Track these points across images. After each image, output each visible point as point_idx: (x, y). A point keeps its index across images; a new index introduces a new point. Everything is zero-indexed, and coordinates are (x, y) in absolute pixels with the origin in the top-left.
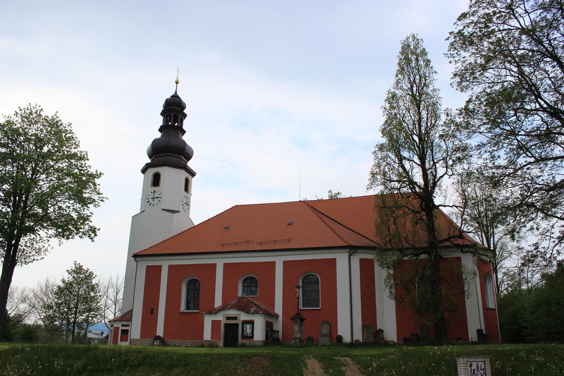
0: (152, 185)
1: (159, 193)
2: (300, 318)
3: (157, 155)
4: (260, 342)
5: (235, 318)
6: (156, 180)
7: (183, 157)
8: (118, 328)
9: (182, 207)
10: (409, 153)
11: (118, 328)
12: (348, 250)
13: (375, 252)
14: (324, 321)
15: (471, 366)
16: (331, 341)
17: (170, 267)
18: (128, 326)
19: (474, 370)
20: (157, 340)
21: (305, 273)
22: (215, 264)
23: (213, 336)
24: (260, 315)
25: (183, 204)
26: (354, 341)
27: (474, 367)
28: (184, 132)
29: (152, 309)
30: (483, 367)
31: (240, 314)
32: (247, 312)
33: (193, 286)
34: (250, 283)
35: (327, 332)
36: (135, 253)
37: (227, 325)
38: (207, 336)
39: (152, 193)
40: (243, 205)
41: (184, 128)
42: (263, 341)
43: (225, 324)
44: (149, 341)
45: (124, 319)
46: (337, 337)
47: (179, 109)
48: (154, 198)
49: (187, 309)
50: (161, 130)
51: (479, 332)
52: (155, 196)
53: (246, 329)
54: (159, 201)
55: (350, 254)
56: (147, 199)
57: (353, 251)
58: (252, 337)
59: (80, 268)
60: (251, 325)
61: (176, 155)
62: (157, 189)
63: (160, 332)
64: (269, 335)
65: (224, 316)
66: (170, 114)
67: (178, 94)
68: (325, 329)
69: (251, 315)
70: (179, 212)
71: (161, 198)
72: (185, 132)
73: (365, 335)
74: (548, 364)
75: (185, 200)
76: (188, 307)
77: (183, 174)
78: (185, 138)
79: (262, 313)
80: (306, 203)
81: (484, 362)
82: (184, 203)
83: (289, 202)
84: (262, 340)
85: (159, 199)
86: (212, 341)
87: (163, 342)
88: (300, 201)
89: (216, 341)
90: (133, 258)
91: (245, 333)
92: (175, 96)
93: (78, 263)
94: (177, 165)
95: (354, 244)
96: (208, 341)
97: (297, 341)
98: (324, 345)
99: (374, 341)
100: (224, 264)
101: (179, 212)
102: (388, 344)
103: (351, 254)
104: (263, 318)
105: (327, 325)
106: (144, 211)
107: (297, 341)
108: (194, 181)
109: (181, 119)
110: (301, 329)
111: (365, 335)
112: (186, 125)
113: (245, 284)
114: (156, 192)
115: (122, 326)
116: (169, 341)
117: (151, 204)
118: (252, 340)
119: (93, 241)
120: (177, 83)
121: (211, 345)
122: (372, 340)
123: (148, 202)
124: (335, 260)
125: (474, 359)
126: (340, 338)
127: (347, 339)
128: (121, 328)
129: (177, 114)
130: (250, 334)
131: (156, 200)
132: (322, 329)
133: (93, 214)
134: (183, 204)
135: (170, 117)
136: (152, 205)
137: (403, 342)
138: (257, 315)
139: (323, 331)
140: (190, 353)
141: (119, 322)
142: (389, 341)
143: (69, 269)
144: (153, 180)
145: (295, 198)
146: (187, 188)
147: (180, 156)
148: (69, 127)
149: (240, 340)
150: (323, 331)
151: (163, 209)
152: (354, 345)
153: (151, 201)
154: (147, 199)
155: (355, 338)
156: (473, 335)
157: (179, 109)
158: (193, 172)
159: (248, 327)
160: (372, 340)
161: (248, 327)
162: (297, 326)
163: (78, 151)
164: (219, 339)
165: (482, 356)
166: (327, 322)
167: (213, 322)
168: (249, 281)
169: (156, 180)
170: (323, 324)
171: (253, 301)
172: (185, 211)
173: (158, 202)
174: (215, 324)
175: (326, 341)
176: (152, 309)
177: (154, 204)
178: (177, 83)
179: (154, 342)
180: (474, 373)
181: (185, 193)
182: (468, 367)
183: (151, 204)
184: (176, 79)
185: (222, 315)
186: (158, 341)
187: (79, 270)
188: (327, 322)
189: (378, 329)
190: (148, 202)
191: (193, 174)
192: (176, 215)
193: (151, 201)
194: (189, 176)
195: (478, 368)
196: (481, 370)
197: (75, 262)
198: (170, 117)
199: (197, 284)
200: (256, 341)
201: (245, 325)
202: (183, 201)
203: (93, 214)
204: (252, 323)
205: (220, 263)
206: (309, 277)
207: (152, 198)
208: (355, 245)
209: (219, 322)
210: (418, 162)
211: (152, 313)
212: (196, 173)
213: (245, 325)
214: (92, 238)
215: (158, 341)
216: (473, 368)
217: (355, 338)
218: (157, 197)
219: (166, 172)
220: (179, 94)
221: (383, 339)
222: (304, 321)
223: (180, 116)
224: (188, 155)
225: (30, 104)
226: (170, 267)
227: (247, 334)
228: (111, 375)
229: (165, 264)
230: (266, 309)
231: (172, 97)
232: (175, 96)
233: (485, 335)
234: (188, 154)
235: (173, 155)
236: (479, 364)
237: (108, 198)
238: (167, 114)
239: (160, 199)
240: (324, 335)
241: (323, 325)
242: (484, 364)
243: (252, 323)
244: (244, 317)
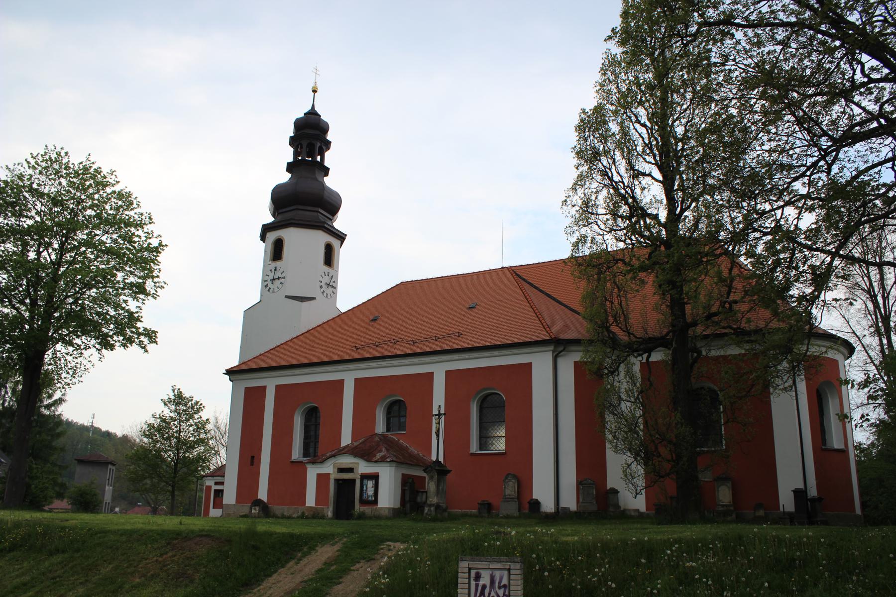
1: (281, 271)
3: (281, 211)
4: (387, 511)
5: (351, 470)
6: (277, 252)
8: (210, 487)
9: (319, 291)
11: (210, 487)
12: (552, 348)
13: (581, 348)
15: (478, 577)
16: (519, 510)
18: (222, 483)
19: (484, 587)
21: (481, 391)
23: (317, 503)
24: (388, 464)
25: (321, 287)
26: (560, 510)
27: (485, 580)
28: (326, 171)
29: (253, 457)
30: (505, 581)
33: (312, 415)
34: (396, 411)
35: (515, 494)
37: (341, 482)
38: (311, 500)
39: (272, 272)
40: (412, 281)
41: (327, 163)
42: (394, 509)
43: (337, 480)
45: (218, 473)
46: (529, 503)
47: (317, 132)
48: (274, 279)
49: (481, 450)
50: (290, 167)
51: (800, 494)
53: (367, 488)
54: (282, 283)
55: (556, 353)
56: (265, 281)
57: (561, 348)
58: (375, 502)
61: (309, 208)
62: (278, 264)
64: (407, 498)
65: (334, 467)
67: (316, 109)
68: (511, 489)
70: (313, 299)
71: (283, 278)
72: (329, 169)
73: (581, 500)
74: (697, 576)
75: (326, 279)
77: (320, 238)
78: (329, 181)
79: (391, 461)
81: (509, 570)
82: (323, 284)
83: (485, 271)
84: (392, 506)
85: (281, 280)
87: (265, 510)
88: (503, 268)
89: (323, 509)
91: (365, 496)
92: (312, 113)
93: (177, 387)
94: (297, 222)
95: (562, 334)
96: (311, 507)
97: (432, 509)
98: (507, 517)
100: (356, 380)
101: (313, 299)
103: (558, 354)
104: (393, 469)
105: (513, 481)
107: (432, 509)
109: (320, 148)
111: (581, 500)
112: (329, 159)
114: (278, 269)
115: (216, 483)
117: (270, 288)
118: (375, 507)
119: (146, 351)
120: (315, 91)
121: (316, 515)
122: (594, 507)
123: (266, 286)
124: (529, 366)
125: (484, 564)
126: (536, 504)
127: (548, 506)
129: (313, 142)
130: (372, 497)
131: (277, 282)
132: (505, 487)
133: (141, 309)
134: (321, 287)
135: (301, 148)
137: (654, 512)
139: (508, 492)
142: (629, 510)
143: (166, 398)
145: (496, 265)
147: (316, 209)
148: (113, 177)
150: (508, 492)
151: (287, 297)
152: (560, 516)
154: (265, 281)
155: (563, 504)
156: (787, 502)
157: (317, 132)
158: (339, 234)
160: (594, 507)
161: (370, 484)
162: (433, 483)
163: (135, 213)
164: (327, 505)
166: (515, 477)
168: (396, 408)
170: (507, 478)
171: (399, 440)
173: (280, 286)
174: (322, 479)
175: (511, 509)
176: (253, 457)
177: (274, 289)
178: (315, 91)
179: (251, 509)
180: (482, 592)
183: (270, 288)
184: (312, 85)
185: (332, 466)
186: (257, 508)
187: (179, 399)
188: (515, 477)
189: (608, 488)
191: (341, 237)
192: (312, 302)
193: (269, 283)
194: (335, 242)
195: (492, 582)
196: (500, 588)
197: (173, 387)
198: (301, 148)
200: (382, 508)
201: (365, 481)
202: (321, 282)
203: (141, 309)
205: (349, 377)
206: (490, 397)
207: (271, 280)
208: (562, 337)
210: (659, 176)
211: (252, 464)
212: (346, 235)
213: (365, 481)
214: (144, 348)
215: (257, 508)
216: (481, 582)
217: (563, 504)
218: (279, 278)
219: (292, 236)
222: (448, 475)
223: (318, 145)
225: (46, 146)
226: (278, 388)
227: (368, 496)
229: (271, 383)
230: (418, 454)
231: (305, 114)
232: (312, 113)
233: (813, 500)
234: (331, 204)
236: (497, 574)
237: (167, 282)
239: (282, 281)
240: (508, 499)
241: (507, 480)
242: (509, 574)
243: (375, 477)
244: (363, 467)
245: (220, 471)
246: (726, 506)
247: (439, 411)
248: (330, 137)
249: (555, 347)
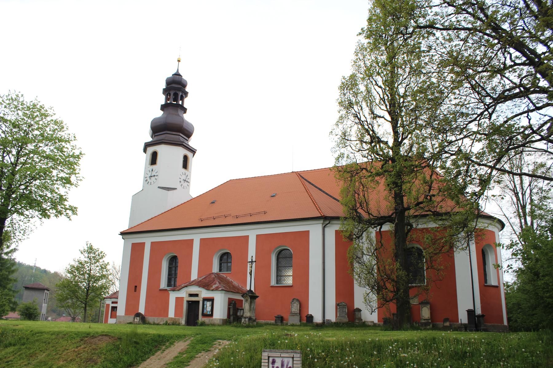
2: (250, 296)
3: (156, 134)
4: (219, 321)
5: (197, 295)
6: (154, 159)
7: (181, 134)
8: (109, 305)
11: (109, 305)
13: (340, 222)
14: (294, 299)
16: (300, 321)
18: (116, 303)
22: (192, 240)
24: (220, 292)
25: (180, 182)
28: (185, 110)
29: (136, 287)
31: (201, 291)
35: (297, 311)
36: (122, 230)
38: (171, 314)
42: (223, 320)
43: (188, 302)
45: (114, 296)
50: (163, 107)
52: (153, 175)
54: (156, 179)
57: (327, 222)
58: (211, 315)
59: (91, 248)
60: (211, 302)
62: (154, 167)
65: (186, 293)
68: (295, 308)
71: (157, 176)
73: (338, 315)
75: (184, 177)
77: (181, 152)
80: (301, 176)
81: (293, 358)
82: (182, 180)
84: (222, 318)
85: (156, 177)
86: (175, 319)
88: (293, 172)
92: (177, 74)
96: (172, 318)
98: (293, 325)
99: (347, 321)
102: (364, 325)
104: (223, 295)
107: (247, 320)
110: (252, 307)
111: (338, 315)
115: (113, 303)
116: (150, 319)
118: (211, 318)
119: (70, 220)
120: (179, 61)
121: (175, 323)
122: (346, 320)
123: (146, 180)
125: (278, 354)
126: (310, 318)
127: (318, 319)
129: (177, 92)
131: (153, 178)
134: (180, 182)
135: (170, 95)
140: (226, 327)
142: (368, 322)
144: (151, 159)
146: (185, 166)
147: (178, 134)
148: (52, 111)
149: (201, 319)
151: (159, 187)
152: (325, 325)
153: (149, 180)
155: (327, 318)
159: (208, 304)
160: (346, 320)
161: (208, 304)
164: (181, 316)
165: (290, 351)
166: (298, 300)
167: (177, 298)
169: (154, 159)
172: (184, 188)
173: (155, 181)
174: (179, 300)
175: (295, 320)
176: (136, 287)
178: (179, 61)
179: (134, 319)
181: (184, 170)
182: (270, 363)
186: (138, 318)
188: (298, 300)
189: (355, 308)
191: (193, 152)
192: (170, 192)
201: (205, 302)
202: (180, 178)
204: (212, 300)
205: (196, 237)
211: (135, 291)
213: (205, 302)
217: (327, 318)
218: (154, 176)
219: (163, 150)
220: (181, 72)
221: (360, 319)
223: (181, 94)
224: (188, 134)
229: (148, 240)
235: (171, 133)
236: (286, 360)
243: (212, 300)
244: (204, 294)
245: (115, 295)
246: (426, 319)
247: (252, 260)
248: (187, 89)
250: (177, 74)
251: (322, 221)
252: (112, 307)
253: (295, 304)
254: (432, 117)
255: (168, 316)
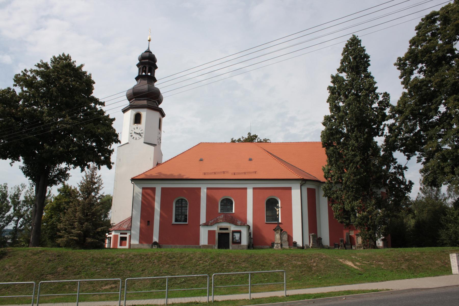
0: (134, 122)
5: (227, 229)
10: (409, 159)
11: (117, 236)
17: (163, 189)
20: (155, 245)
29: (149, 222)
31: (230, 226)
32: (236, 224)
33: (181, 204)
36: (132, 177)
42: (247, 245)
43: (219, 233)
44: (146, 246)
47: (153, 62)
55: (301, 184)
56: (131, 133)
63: (156, 239)
65: (218, 227)
66: (146, 66)
69: (240, 227)
76: (176, 220)
77: (157, 114)
90: (131, 181)
92: (148, 51)
106: (128, 143)
108: (164, 120)
113: (223, 204)
114: (138, 128)
115: (121, 234)
118: (240, 245)
123: (132, 136)
126: (295, 244)
127: (300, 243)
128: (120, 236)
129: (152, 67)
136: (135, 138)
138: (244, 227)
141: (119, 231)
144: (134, 119)
157: (153, 62)
176: (149, 222)
177: (136, 138)
178: (149, 41)
190: (132, 136)
199: (183, 203)
204: (240, 232)
209: (214, 231)
220: (151, 50)
228: (452, 228)
229: (159, 187)
238: (144, 66)
243: (240, 232)
244: (233, 228)
246: (360, 244)
248: (157, 64)
249: (302, 182)
250: (148, 51)
251: (300, 182)
252: (121, 238)
253: (285, 235)
254: (435, 134)
255: (199, 244)
